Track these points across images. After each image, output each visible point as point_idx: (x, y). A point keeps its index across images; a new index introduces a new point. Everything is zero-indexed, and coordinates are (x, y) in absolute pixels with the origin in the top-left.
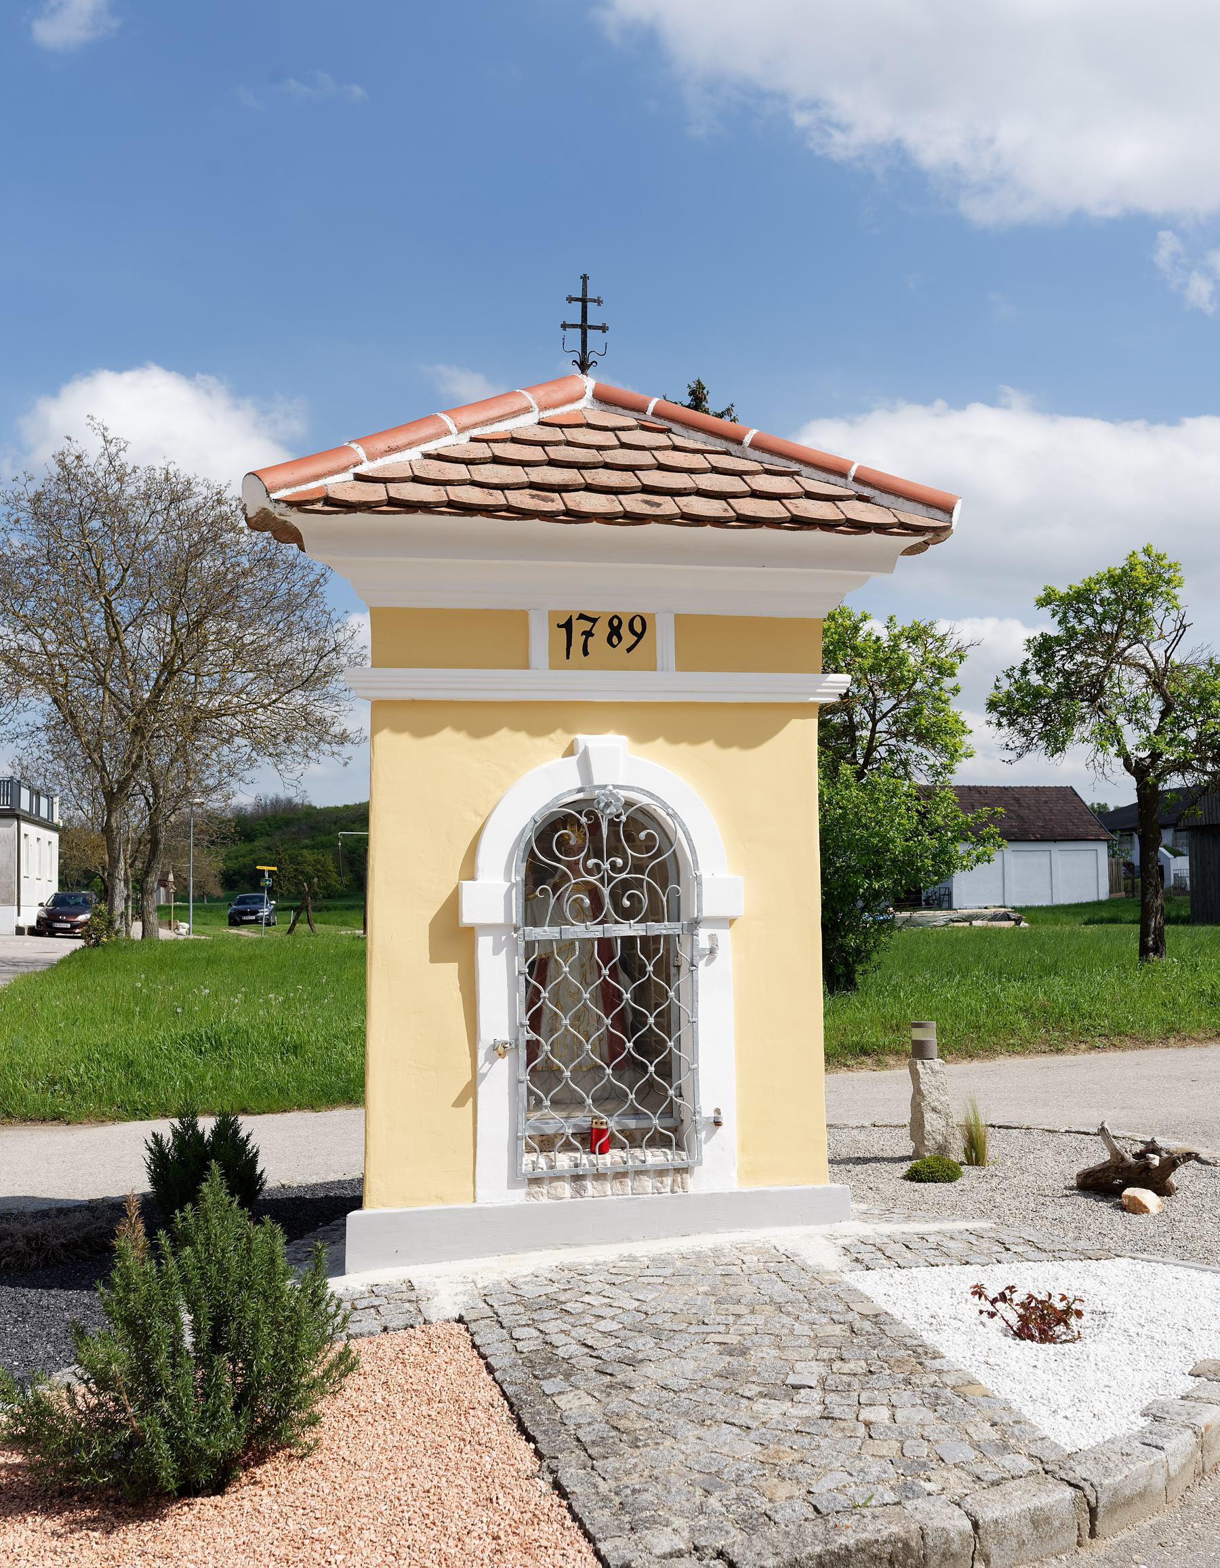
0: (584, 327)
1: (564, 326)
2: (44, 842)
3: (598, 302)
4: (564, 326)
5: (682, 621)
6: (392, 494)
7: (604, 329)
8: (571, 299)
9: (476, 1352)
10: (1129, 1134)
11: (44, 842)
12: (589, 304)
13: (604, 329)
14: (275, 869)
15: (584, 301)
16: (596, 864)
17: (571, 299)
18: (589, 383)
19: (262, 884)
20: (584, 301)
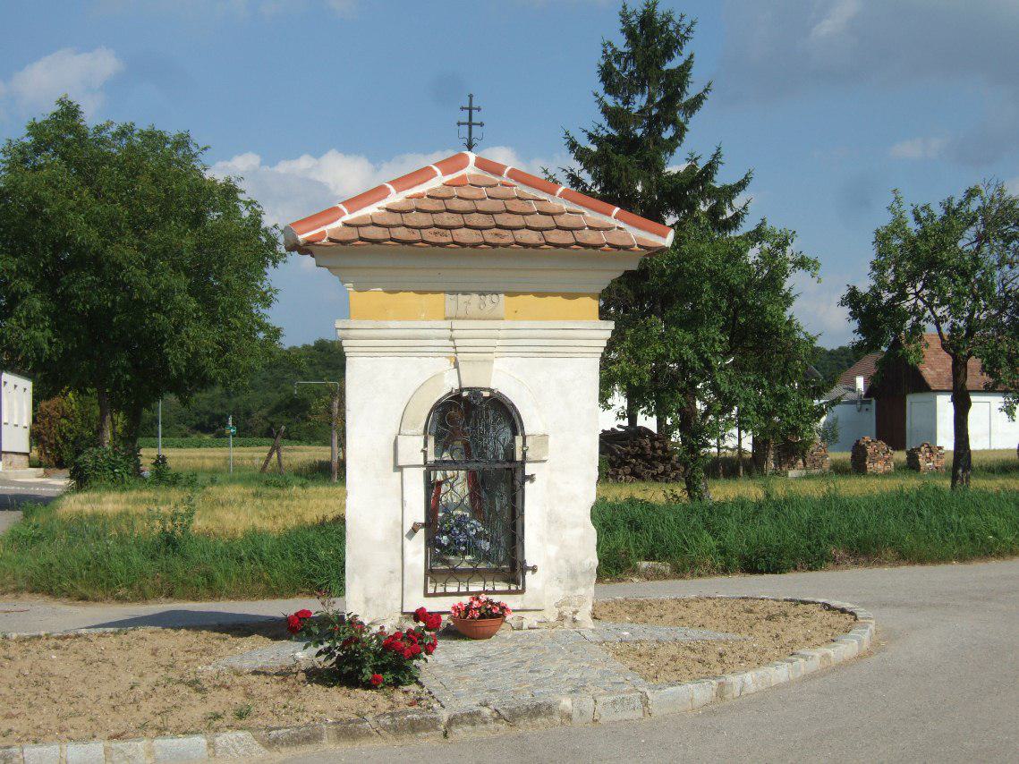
0: (470, 124)
1: (459, 124)
2: (20, 388)
3: (479, 109)
4: (459, 124)
5: (392, 183)
6: (362, 235)
7: (482, 125)
8: (462, 109)
9: (72, 634)
10: (847, 605)
11: (20, 388)
12: (473, 111)
13: (482, 125)
14: (230, 418)
15: (470, 110)
16: (475, 433)
17: (462, 109)
18: (472, 156)
19: (227, 432)
20: (470, 110)
